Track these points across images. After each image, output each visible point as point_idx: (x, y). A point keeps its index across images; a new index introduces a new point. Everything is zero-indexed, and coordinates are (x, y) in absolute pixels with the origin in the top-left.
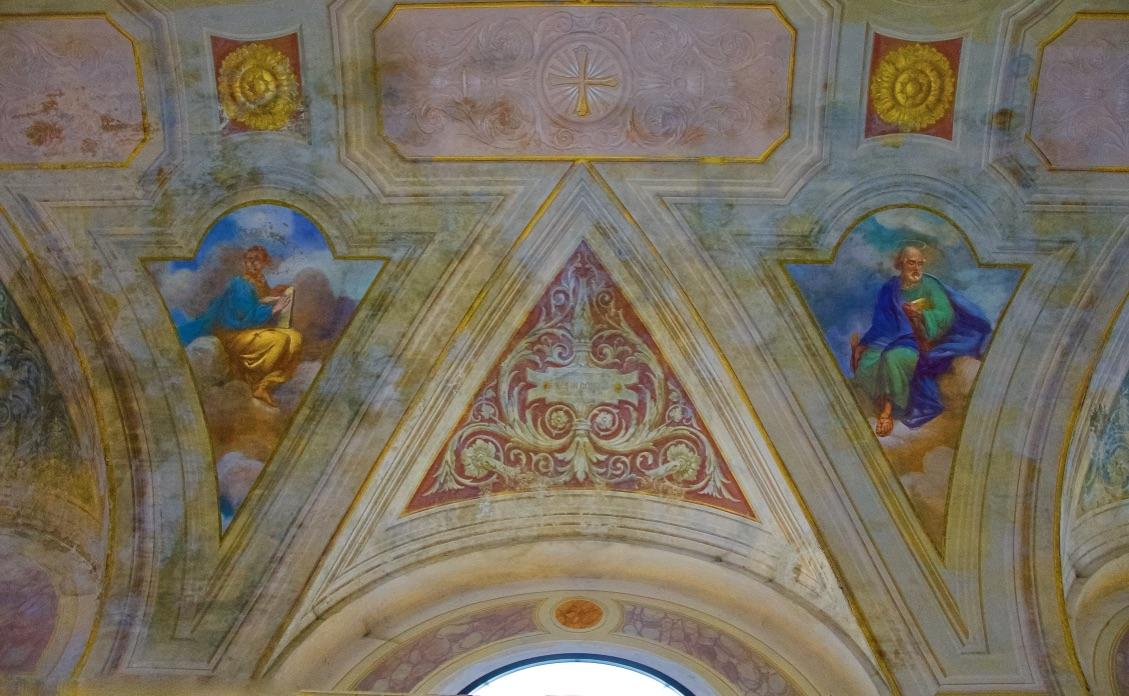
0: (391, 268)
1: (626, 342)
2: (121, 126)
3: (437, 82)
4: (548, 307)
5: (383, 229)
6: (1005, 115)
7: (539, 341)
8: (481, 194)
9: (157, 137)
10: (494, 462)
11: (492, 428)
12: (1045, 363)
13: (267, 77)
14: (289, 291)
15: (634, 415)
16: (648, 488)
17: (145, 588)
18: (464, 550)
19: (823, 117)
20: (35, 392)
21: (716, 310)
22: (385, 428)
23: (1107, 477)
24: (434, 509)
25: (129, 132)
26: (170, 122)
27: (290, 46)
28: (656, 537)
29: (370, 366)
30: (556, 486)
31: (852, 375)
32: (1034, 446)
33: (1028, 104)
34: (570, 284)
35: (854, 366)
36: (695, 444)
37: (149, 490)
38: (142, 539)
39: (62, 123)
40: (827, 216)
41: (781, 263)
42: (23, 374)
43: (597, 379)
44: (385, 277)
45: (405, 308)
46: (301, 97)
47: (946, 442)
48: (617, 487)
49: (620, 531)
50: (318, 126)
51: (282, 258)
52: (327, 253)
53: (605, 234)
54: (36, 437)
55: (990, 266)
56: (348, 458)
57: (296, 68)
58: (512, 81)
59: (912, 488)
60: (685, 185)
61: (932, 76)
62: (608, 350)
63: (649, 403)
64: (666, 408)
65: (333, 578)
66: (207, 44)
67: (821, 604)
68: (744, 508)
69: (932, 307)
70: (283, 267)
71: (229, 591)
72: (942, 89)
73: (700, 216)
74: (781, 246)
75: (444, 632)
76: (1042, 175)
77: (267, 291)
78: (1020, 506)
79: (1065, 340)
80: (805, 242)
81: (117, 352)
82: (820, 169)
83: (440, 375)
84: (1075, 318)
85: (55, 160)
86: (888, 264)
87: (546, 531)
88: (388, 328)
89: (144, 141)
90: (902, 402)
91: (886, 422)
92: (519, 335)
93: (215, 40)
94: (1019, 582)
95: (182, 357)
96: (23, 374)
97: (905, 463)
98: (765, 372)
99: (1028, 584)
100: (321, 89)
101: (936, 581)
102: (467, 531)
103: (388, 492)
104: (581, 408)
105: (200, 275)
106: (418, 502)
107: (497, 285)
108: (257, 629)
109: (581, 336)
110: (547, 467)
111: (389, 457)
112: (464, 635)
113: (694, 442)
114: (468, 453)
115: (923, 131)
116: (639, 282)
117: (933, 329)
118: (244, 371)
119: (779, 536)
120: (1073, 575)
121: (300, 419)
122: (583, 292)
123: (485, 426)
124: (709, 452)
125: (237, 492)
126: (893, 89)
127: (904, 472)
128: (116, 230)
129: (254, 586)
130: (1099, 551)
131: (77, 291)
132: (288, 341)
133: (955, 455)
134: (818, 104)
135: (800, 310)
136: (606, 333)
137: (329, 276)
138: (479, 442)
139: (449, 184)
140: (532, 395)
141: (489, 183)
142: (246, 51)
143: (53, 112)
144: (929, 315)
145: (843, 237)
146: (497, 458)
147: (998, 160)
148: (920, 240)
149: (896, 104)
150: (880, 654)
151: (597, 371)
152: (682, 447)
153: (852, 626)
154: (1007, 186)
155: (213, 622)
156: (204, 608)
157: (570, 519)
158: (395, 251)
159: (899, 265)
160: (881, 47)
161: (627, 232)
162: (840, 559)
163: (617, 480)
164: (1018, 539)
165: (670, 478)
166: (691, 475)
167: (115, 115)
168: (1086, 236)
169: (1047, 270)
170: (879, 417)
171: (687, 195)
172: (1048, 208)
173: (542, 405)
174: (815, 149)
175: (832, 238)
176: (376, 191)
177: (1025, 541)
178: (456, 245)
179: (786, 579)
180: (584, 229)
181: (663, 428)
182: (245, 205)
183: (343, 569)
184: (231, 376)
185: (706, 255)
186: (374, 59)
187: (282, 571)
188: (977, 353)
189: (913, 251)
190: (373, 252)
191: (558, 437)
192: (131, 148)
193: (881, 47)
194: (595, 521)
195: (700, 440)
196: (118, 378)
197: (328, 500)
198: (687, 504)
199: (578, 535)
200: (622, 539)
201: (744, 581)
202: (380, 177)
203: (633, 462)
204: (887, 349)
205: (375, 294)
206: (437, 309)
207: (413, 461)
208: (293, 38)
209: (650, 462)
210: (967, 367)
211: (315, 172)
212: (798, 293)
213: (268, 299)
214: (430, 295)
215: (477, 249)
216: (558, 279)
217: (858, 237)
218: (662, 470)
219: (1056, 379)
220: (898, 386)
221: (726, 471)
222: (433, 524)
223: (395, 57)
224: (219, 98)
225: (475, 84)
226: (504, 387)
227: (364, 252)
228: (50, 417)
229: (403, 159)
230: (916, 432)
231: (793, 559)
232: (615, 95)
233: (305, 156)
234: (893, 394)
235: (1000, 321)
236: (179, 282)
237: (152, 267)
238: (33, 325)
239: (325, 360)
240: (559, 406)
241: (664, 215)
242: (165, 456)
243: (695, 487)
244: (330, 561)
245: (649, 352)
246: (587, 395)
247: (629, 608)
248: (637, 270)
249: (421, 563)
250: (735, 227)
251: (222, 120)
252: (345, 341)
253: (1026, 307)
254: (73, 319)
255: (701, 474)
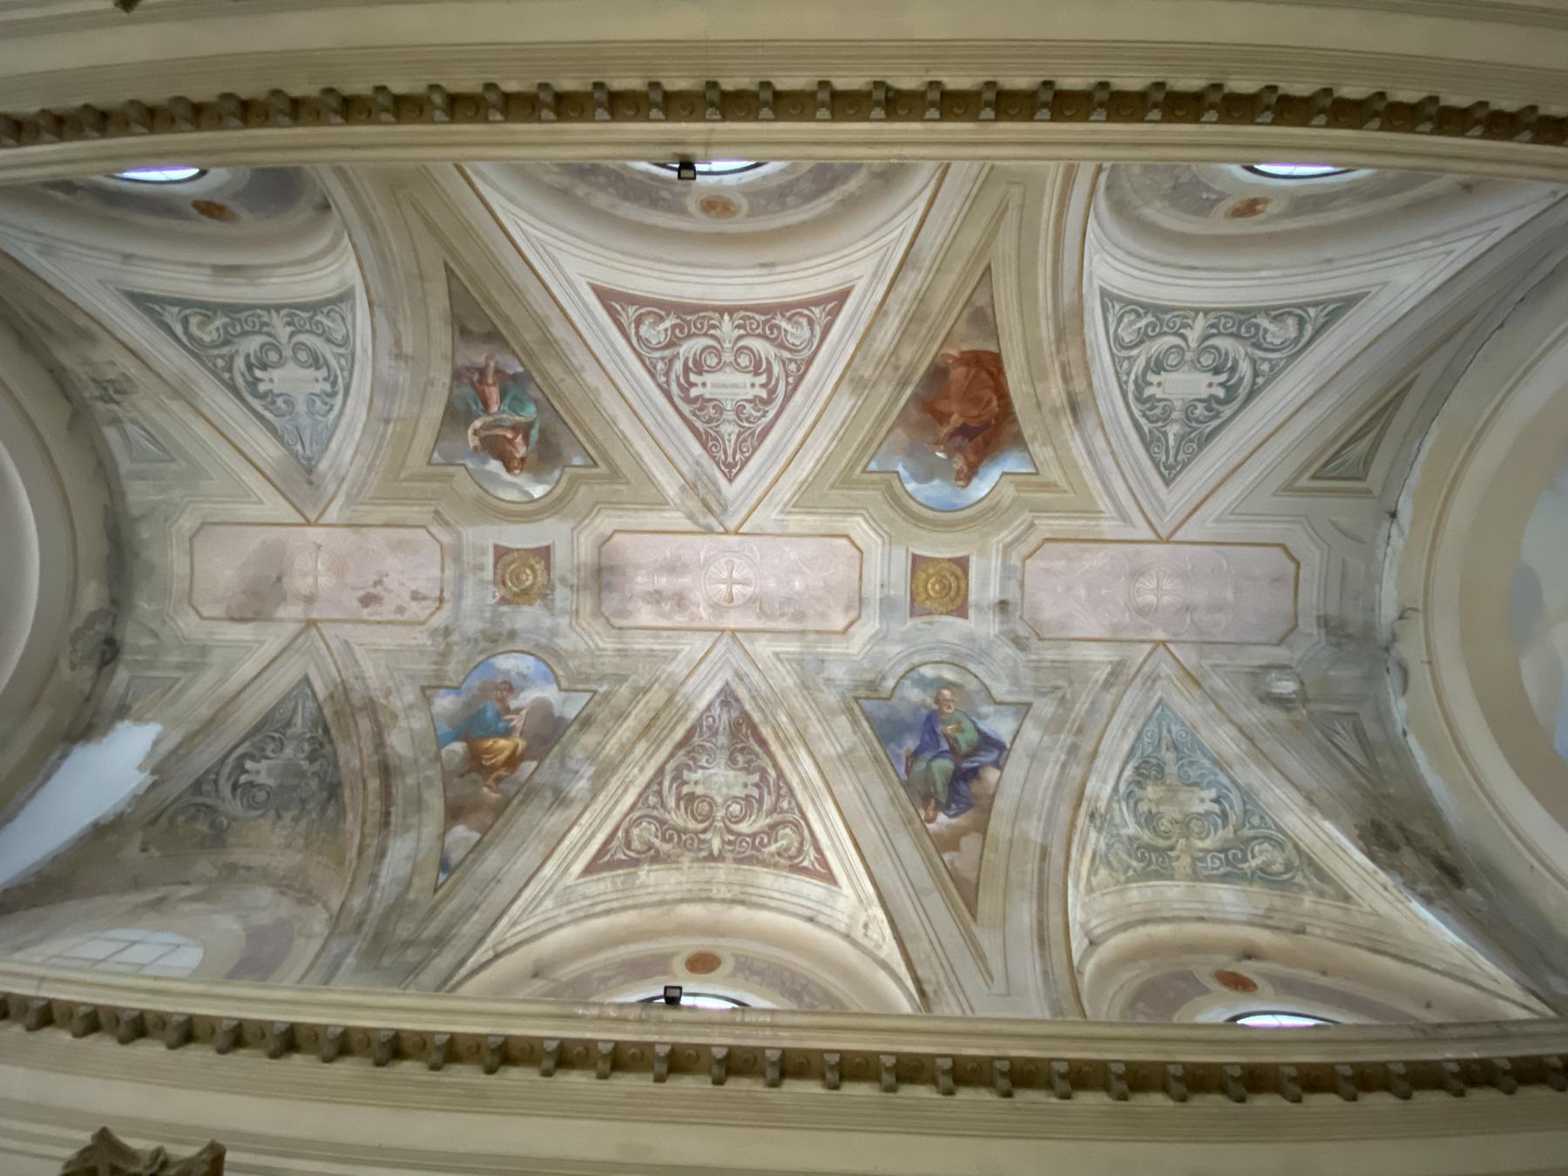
0: (597, 698)
1: (753, 752)
2: (425, 598)
3: (639, 579)
4: (701, 726)
5: (593, 672)
6: (1003, 605)
7: (693, 750)
8: (662, 651)
9: (447, 606)
10: (789, 328)
11: (655, 813)
12: (1050, 773)
13: (528, 571)
14: (524, 713)
15: (756, 805)
16: (763, 863)
17: (365, 928)
18: (624, 909)
19: (881, 603)
20: (321, 781)
21: (812, 730)
22: (576, 810)
23: (1109, 865)
24: (604, 874)
25: (429, 603)
26: (459, 596)
27: (545, 553)
28: (767, 901)
29: (572, 764)
30: (697, 860)
31: (906, 778)
32: (1045, 835)
33: (1018, 596)
34: (716, 711)
35: (908, 771)
36: (797, 825)
37: (389, 854)
38: (373, 892)
39: (383, 593)
40: (887, 668)
41: (856, 699)
42: (316, 767)
43: (731, 779)
44: (592, 704)
45: (603, 725)
46: (550, 586)
47: (977, 830)
48: (739, 861)
49: (741, 897)
50: (559, 603)
51: (522, 689)
52: (554, 688)
53: (741, 679)
54: (314, 815)
55: (1001, 703)
56: (544, 832)
57: (548, 568)
58: (685, 581)
59: (952, 863)
60: (793, 647)
61: (952, 579)
62: (740, 758)
63: (766, 798)
64: (777, 800)
65: (514, 924)
66: (491, 551)
67: (882, 954)
68: (830, 878)
69: (960, 730)
70: (523, 695)
71: (432, 929)
72: (959, 588)
73: (802, 667)
74: (856, 688)
75: (596, 975)
76: (1034, 641)
77: (508, 711)
78: (1036, 880)
79: (1063, 757)
80: (873, 686)
81: (388, 750)
82: (880, 638)
83: (621, 772)
84: (1069, 741)
85: (373, 618)
86: (929, 701)
87: (686, 895)
88: (589, 739)
89: (438, 608)
90: (943, 799)
91: (931, 813)
92: (680, 745)
93: (496, 547)
94: (1035, 940)
95: (438, 757)
96: (316, 767)
97: (948, 842)
98: (843, 773)
99: (1042, 941)
100: (563, 581)
101: (970, 937)
102: (627, 893)
103: (570, 857)
104: (719, 800)
105: (463, 698)
106: (590, 869)
107: (667, 711)
108: (445, 960)
109: (722, 747)
110: (692, 844)
111: (575, 831)
112: (609, 978)
113: (796, 826)
114: (635, 831)
115: (948, 614)
116: (762, 711)
117: (964, 747)
118: (482, 766)
119: (853, 898)
120: (1086, 942)
121: (515, 802)
122: (725, 717)
123: (200, 800)
124: (806, 833)
125: (455, 857)
126: (926, 588)
127: (947, 850)
128: (406, 666)
129: (452, 927)
130: (1109, 926)
131: (371, 706)
132: (517, 746)
133: (984, 839)
134: (878, 596)
135: (869, 731)
136: (739, 746)
137: (553, 701)
138: (644, 824)
139: (642, 643)
140: (685, 790)
141: (668, 644)
142: (516, 555)
143: (379, 587)
144: (959, 736)
145: (898, 683)
146: (656, 836)
147: (1002, 633)
148: (950, 685)
149: (929, 597)
150: (922, 993)
151: (731, 773)
152: (788, 831)
153: (903, 971)
154: (1009, 650)
155: (412, 955)
156: (407, 944)
157: (706, 887)
158: (601, 686)
159: (937, 701)
160: (917, 561)
161: (755, 677)
162: (897, 920)
163: (741, 856)
164: (1035, 904)
165: (779, 854)
166: (793, 851)
167: (421, 591)
168: (1071, 683)
169: (1045, 708)
170: (926, 809)
171: (794, 653)
172: (1043, 664)
173: (692, 797)
174: (877, 625)
175: (890, 683)
176: (593, 647)
177: (1041, 908)
178: (642, 683)
179: (858, 934)
180: (728, 675)
181: (775, 816)
182: (502, 653)
183: (524, 917)
184: (470, 771)
185: (805, 692)
186: (599, 563)
187: (476, 917)
188: (998, 765)
189: (946, 693)
190: (586, 687)
191: (702, 821)
192: (428, 612)
193: (917, 561)
194: (723, 889)
195: (801, 824)
196: (386, 771)
197: (524, 862)
198: (791, 875)
199: (710, 900)
200: (742, 903)
201: (827, 936)
202: (597, 638)
203: (753, 842)
204: (931, 760)
205: (584, 714)
206: (625, 726)
207: (593, 835)
208: (548, 548)
209: (766, 841)
210: (992, 775)
211: (554, 633)
212: (867, 719)
213: (508, 717)
214: (621, 716)
215: (656, 686)
216: (709, 708)
217: (907, 682)
218: (773, 848)
219: (1058, 786)
220: (940, 787)
221: (818, 850)
222: (601, 887)
223: (612, 563)
224: (495, 583)
225: (663, 582)
226: (666, 783)
227: (580, 686)
228: (329, 799)
229: (613, 627)
230: (954, 821)
231: (863, 918)
232: (749, 590)
233: (547, 622)
234: (936, 792)
235: (1012, 742)
236: (445, 703)
237: (428, 692)
238: (333, 732)
239: (541, 760)
240: (704, 798)
241: (779, 665)
242: (407, 828)
243: (796, 861)
244: (515, 910)
245: (767, 760)
246: (724, 791)
247: (743, 960)
248: (761, 702)
249: (588, 917)
250: (825, 675)
251: (494, 597)
252: (556, 748)
253: (1031, 733)
254: (365, 725)
255: (800, 850)
